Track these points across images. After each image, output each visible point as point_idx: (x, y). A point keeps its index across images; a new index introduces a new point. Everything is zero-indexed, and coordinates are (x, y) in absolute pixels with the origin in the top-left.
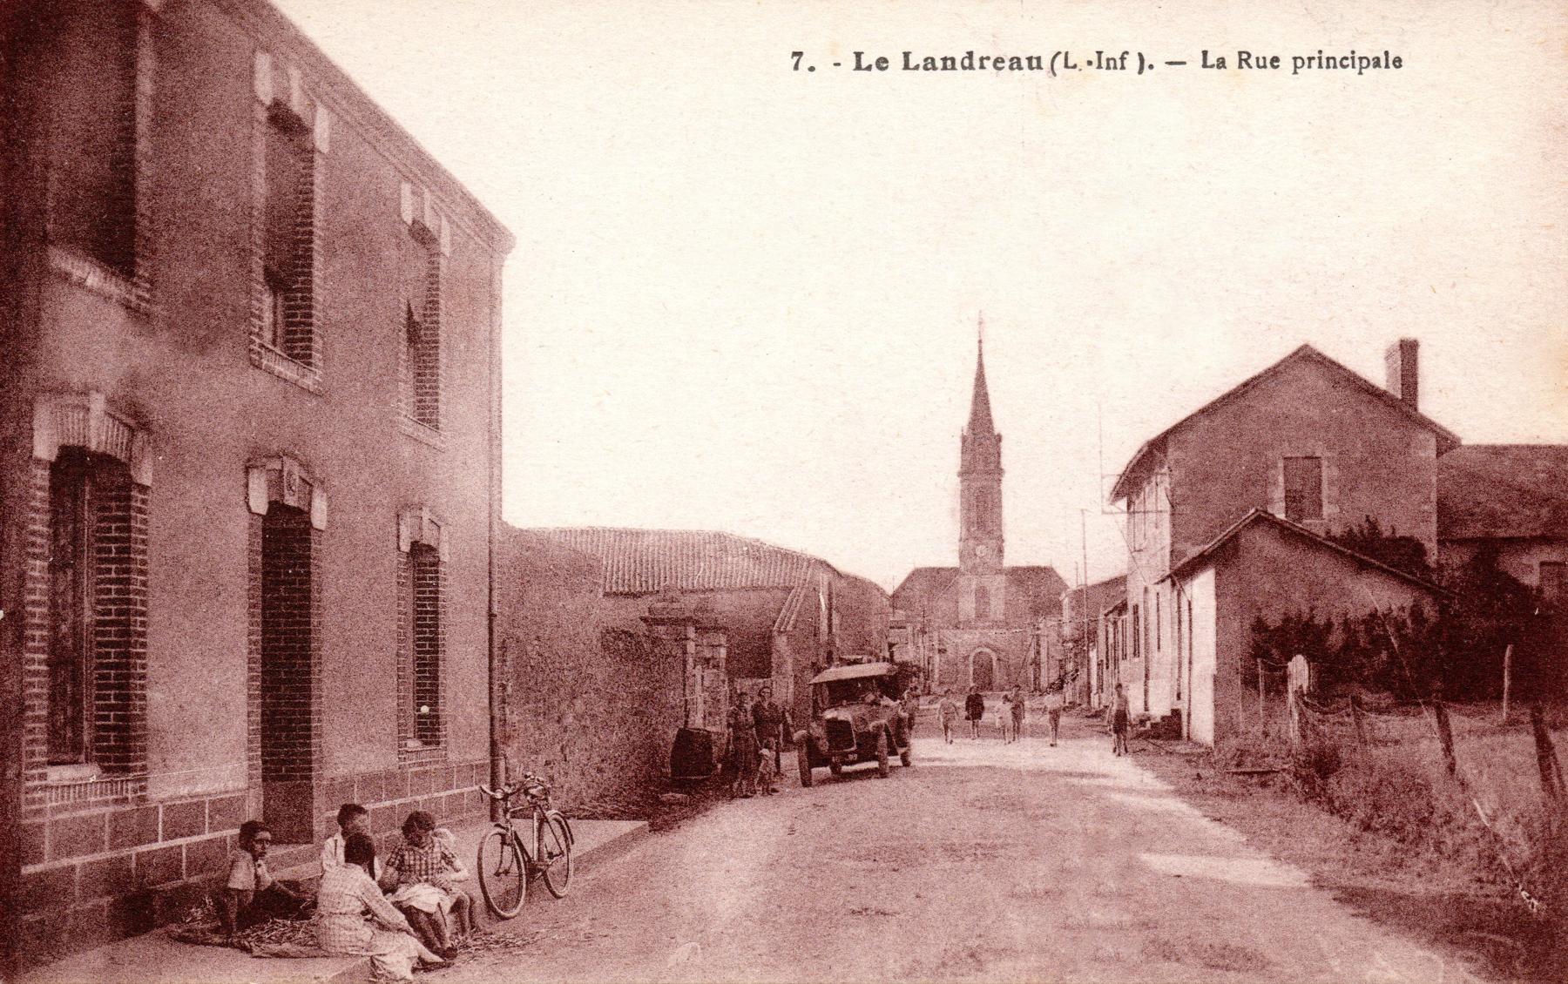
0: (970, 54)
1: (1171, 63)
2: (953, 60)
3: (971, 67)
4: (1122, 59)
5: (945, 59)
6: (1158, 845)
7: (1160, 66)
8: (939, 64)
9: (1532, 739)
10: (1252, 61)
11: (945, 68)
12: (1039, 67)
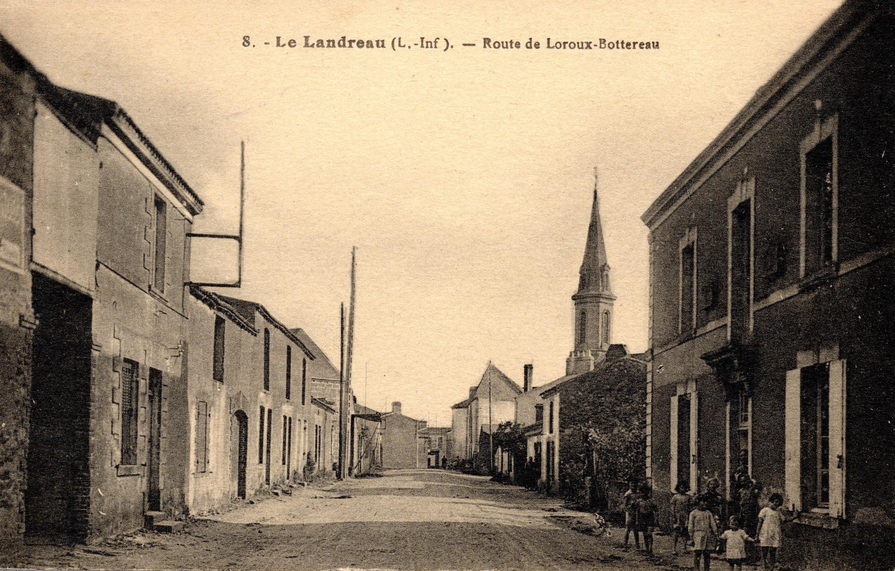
0: (344, 38)
1: (465, 45)
2: (333, 41)
3: (344, 46)
4: (436, 42)
5: (329, 41)
6: (135, 180)
7: (459, 47)
8: (325, 44)
9: (530, 424)
10: (491, 44)
11: (329, 46)
12: (383, 46)
